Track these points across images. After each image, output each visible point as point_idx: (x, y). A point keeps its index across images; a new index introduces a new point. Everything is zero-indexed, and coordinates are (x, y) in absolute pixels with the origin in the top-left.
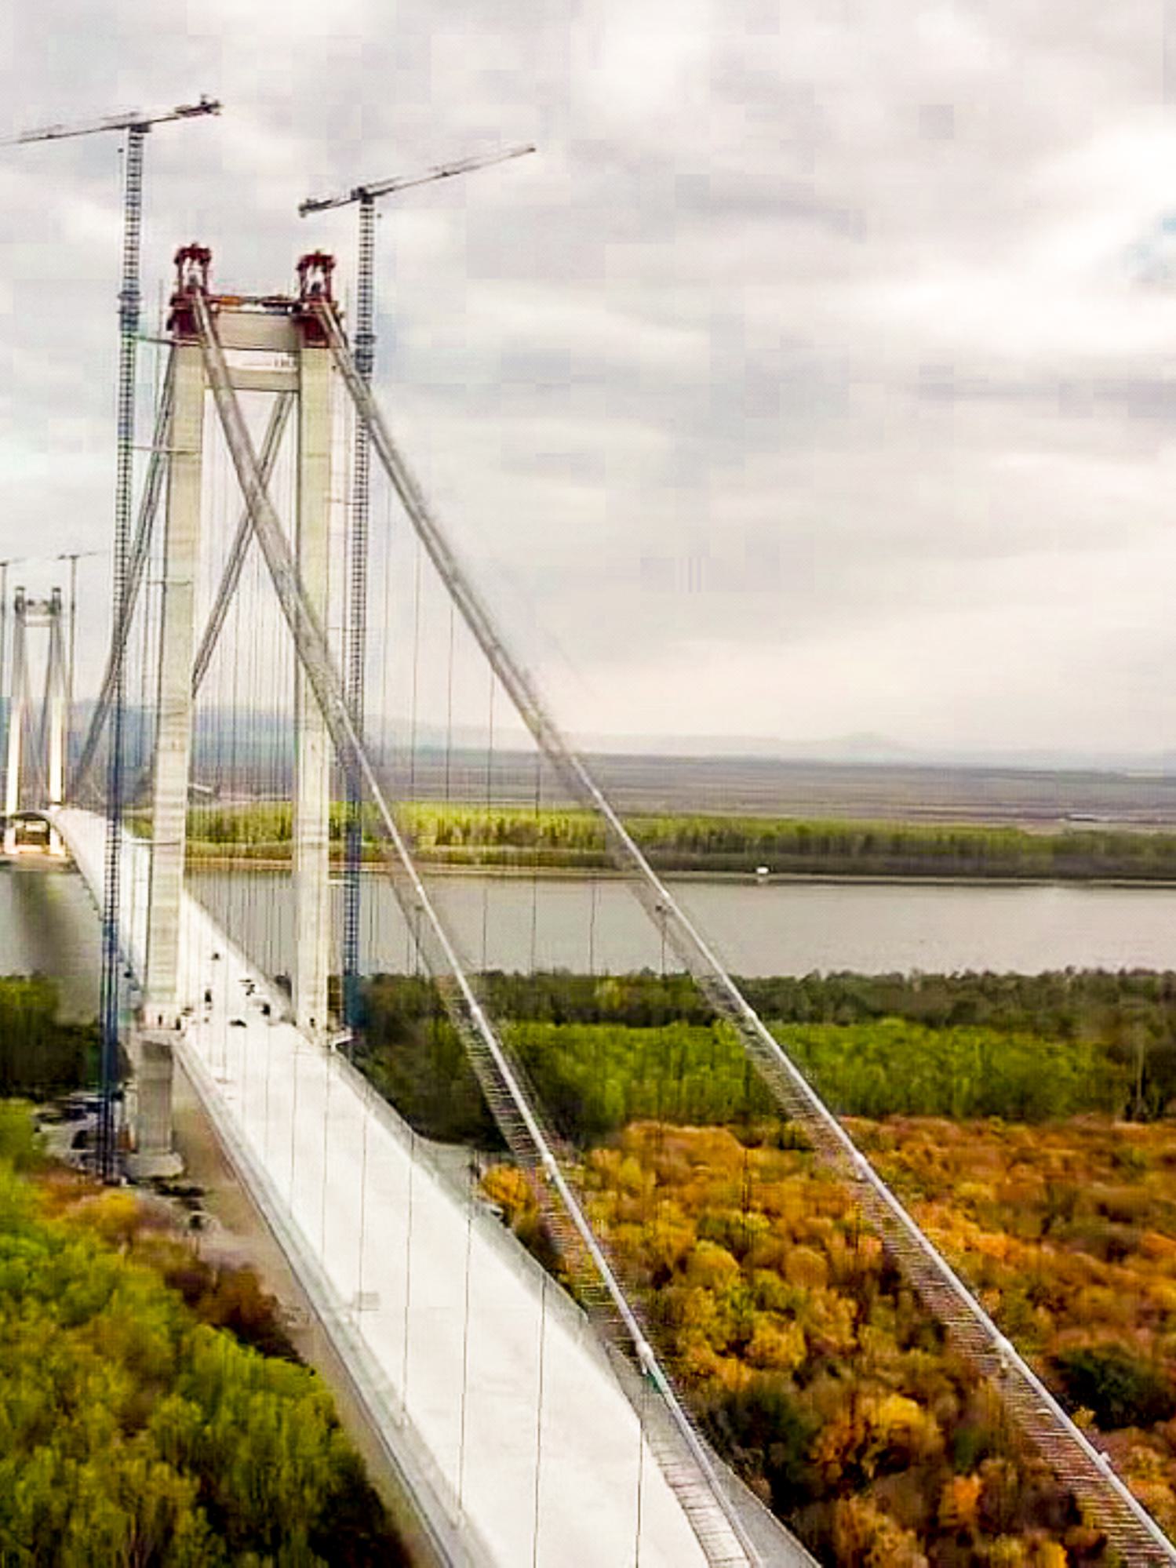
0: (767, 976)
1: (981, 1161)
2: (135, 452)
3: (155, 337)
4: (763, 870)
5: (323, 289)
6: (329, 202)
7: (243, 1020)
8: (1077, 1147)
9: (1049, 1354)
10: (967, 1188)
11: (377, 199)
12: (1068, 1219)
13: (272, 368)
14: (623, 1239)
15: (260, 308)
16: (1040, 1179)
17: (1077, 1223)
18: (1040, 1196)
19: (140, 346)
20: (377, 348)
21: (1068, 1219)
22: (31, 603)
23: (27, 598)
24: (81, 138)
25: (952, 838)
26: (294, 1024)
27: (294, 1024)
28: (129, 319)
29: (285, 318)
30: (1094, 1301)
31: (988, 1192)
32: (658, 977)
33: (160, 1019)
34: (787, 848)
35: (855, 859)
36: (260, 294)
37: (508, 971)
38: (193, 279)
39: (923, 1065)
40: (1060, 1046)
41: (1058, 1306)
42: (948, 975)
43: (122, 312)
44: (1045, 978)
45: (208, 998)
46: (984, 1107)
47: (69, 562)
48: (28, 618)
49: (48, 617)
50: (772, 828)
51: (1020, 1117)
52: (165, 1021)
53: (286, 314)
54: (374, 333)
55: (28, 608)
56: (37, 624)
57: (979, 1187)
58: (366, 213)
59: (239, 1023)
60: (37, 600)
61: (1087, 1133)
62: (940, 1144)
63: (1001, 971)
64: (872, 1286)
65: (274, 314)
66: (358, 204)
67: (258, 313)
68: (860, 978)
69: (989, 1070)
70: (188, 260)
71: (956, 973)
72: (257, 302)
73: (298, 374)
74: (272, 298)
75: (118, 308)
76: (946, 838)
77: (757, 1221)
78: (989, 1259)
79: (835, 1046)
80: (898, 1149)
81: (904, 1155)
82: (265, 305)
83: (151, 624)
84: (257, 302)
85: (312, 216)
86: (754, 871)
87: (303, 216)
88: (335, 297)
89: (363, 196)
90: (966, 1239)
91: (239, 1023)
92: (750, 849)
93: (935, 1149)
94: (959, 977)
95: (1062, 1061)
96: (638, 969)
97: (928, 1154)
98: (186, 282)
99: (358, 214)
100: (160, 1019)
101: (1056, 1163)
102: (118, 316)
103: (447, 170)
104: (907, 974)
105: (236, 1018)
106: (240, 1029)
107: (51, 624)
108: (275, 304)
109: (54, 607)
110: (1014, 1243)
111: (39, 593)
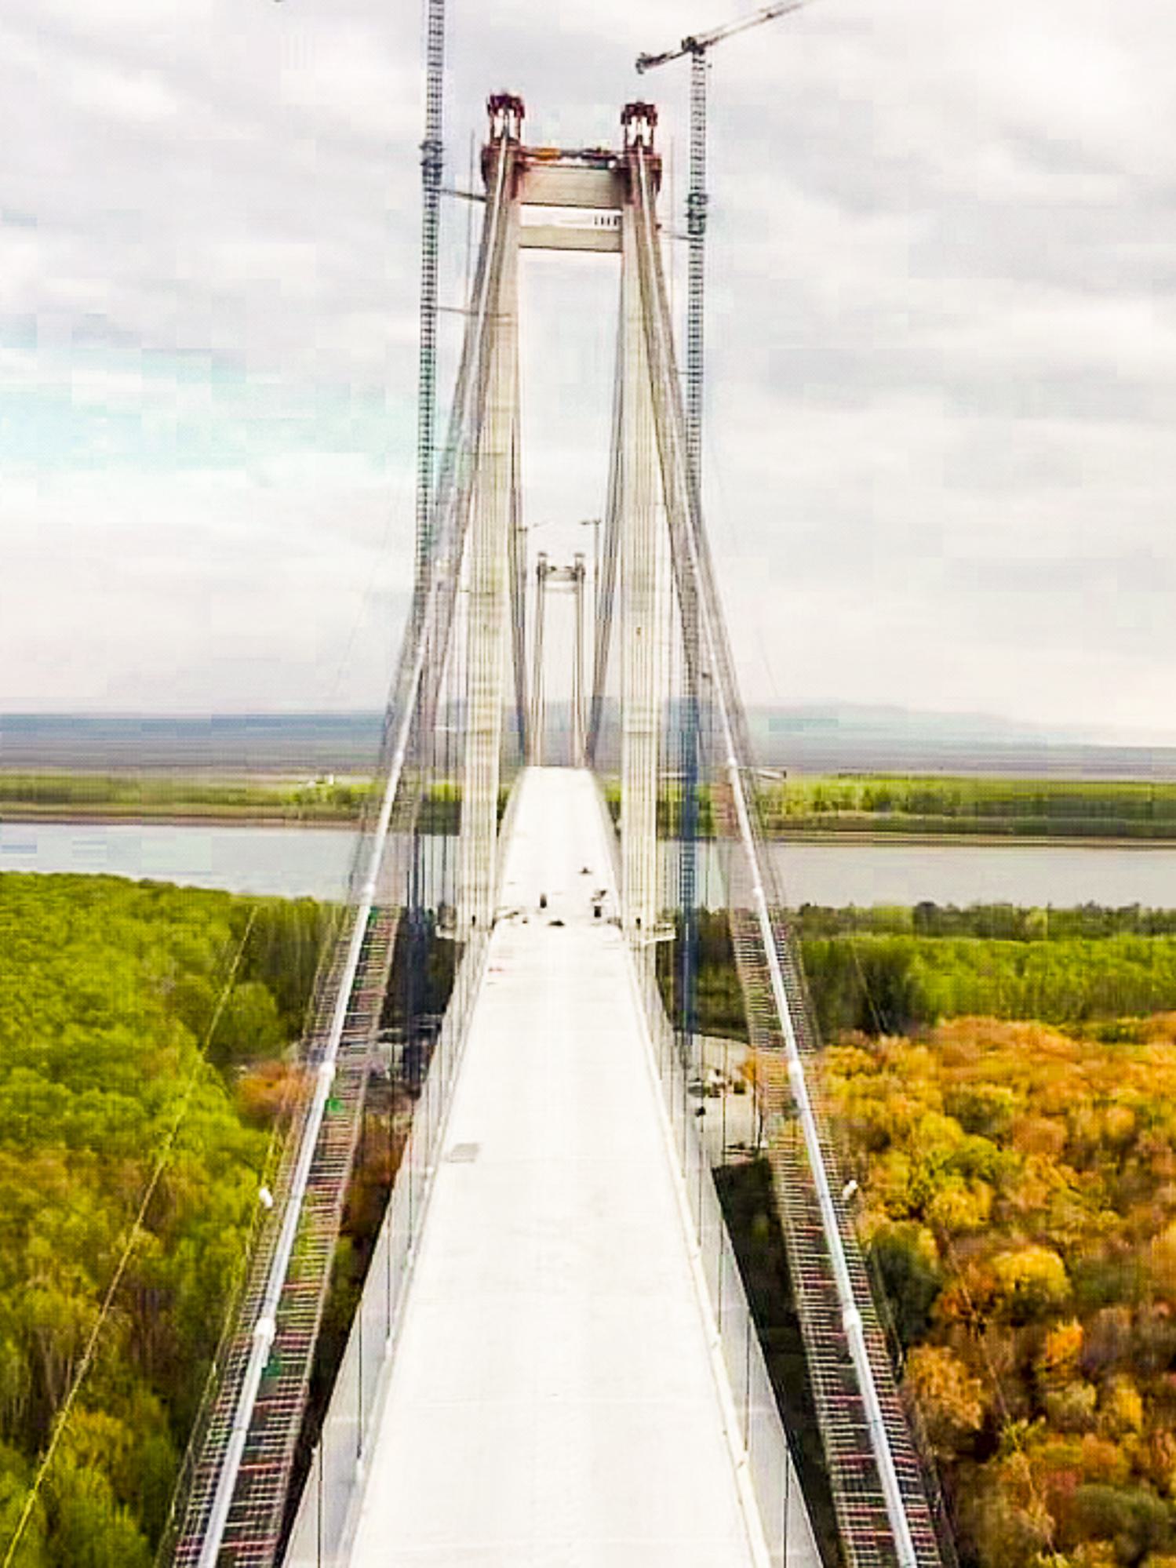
2: (439, 313)
3: (467, 191)
5: (646, 142)
6: (663, 56)
11: (708, 49)
13: (592, 226)
14: (457, 939)
15: (579, 161)
19: (444, 200)
20: (709, 208)
22: (553, 569)
23: (550, 563)
24: (711, 146)
26: (620, 926)
27: (620, 926)
28: (432, 168)
29: (605, 172)
33: (474, 919)
36: (577, 148)
37: (941, 903)
38: (639, 138)
43: (424, 164)
45: (543, 904)
49: (571, 584)
53: (606, 168)
54: (707, 192)
55: (548, 577)
56: (557, 590)
58: (699, 66)
59: (559, 924)
60: (560, 565)
65: (591, 167)
66: (689, 55)
67: (577, 167)
70: (634, 119)
72: (574, 156)
74: (589, 151)
75: (421, 160)
82: (584, 158)
84: (574, 156)
85: (651, 71)
87: (641, 72)
88: (656, 150)
89: (693, 46)
91: (559, 924)
98: (631, 142)
99: (691, 65)
100: (474, 919)
102: (421, 168)
103: (773, 11)
105: (555, 919)
106: (556, 929)
107: (575, 590)
108: (597, 157)
109: (576, 574)
111: (560, 559)
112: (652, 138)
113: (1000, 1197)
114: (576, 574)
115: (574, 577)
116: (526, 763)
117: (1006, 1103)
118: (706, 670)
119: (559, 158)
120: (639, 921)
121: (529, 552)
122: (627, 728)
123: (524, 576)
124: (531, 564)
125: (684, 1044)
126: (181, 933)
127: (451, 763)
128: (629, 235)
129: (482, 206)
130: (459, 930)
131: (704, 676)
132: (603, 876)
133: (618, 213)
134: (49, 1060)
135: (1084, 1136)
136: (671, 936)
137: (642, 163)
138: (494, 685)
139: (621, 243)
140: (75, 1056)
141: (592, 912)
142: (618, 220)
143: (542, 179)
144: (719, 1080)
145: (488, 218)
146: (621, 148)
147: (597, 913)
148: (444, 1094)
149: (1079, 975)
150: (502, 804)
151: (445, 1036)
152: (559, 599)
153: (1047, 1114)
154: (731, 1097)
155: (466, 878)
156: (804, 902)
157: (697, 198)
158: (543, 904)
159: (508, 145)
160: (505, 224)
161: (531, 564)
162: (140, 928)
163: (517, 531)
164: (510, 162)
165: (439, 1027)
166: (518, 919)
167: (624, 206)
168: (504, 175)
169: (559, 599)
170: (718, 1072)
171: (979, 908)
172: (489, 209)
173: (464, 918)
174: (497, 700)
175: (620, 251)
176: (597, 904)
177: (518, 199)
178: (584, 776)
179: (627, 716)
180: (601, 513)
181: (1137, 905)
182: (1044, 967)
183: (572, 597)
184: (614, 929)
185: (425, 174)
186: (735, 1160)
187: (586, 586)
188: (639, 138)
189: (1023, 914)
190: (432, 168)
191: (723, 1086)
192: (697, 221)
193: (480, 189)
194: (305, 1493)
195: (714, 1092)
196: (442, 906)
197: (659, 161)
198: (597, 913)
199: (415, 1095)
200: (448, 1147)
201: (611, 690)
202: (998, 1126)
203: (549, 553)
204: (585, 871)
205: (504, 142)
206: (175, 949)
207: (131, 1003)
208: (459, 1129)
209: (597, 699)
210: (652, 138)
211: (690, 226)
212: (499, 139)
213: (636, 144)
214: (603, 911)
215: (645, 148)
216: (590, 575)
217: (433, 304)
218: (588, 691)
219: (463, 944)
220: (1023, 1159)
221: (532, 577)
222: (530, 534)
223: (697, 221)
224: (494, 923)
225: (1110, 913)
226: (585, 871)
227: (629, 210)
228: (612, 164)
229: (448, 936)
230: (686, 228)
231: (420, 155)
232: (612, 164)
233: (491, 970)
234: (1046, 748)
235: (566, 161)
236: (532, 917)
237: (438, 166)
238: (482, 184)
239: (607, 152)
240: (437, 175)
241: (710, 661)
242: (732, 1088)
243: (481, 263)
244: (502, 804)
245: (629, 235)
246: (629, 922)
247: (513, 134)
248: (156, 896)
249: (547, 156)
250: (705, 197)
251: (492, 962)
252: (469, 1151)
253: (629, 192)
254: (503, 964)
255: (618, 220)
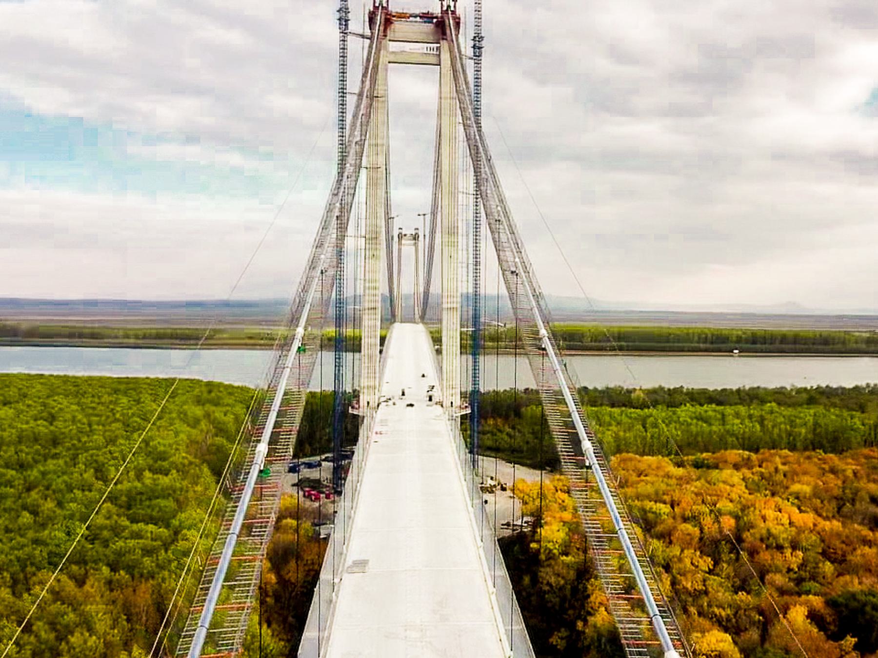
0: (719, 389)
1: (805, 473)
2: (347, 95)
4: (736, 351)
7: (413, 403)
8: (861, 465)
9: (829, 597)
10: (796, 487)
12: (853, 505)
14: (360, 414)
15: (418, 19)
16: (840, 483)
17: (858, 505)
18: (837, 492)
19: (349, 38)
21: (853, 505)
22: (405, 235)
23: (403, 233)
25: (821, 336)
26: (442, 406)
27: (442, 406)
28: (344, 22)
30: (863, 555)
31: (807, 489)
32: (666, 389)
33: (368, 403)
34: (747, 341)
35: (777, 345)
36: (417, 12)
37: (591, 387)
38: (449, 7)
39: (781, 423)
40: (858, 414)
41: (840, 561)
42: (809, 388)
43: (340, 19)
44: (856, 388)
45: (403, 394)
46: (814, 444)
47: (422, 217)
48: (403, 242)
49: (414, 241)
50: (740, 333)
51: (834, 451)
52: (371, 404)
54: (483, 35)
55: (404, 237)
57: (803, 487)
59: (412, 405)
60: (408, 233)
61: (867, 457)
62: (784, 464)
63: (835, 386)
64: (725, 547)
65: (425, 22)
68: (765, 389)
69: (816, 424)
71: (812, 387)
72: (416, 17)
73: (439, 55)
74: (423, 13)
76: (818, 336)
77: (665, 509)
78: (800, 531)
79: (737, 415)
80: (760, 466)
81: (763, 470)
82: (421, 17)
83: (465, 247)
86: (732, 352)
90: (790, 518)
91: (412, 405)
92: (732, 342)
93: (780, 467)
94: (814, 388)
95: (856, 420)
96: (657, 386)
97: (777, 470)
98: (445, 8)
100: (368, 403)
101: (849, 473)
102: (338, 22)
104: (789, 388)
105: (409, 403)
106: (410, 408)
108: (427, 17)
109: (415, 237)
110: (819, 520)
112: (455, 7)
113: (673, 583)
114: (415, 237)
115: (415, 239)
116: (395, 321)
117: (662, 512)
118: (513, 269)
119: (409, 18)
120: (452, 403)
121: (394, 228)
122: (445, 306)
123: (392, 239)
124: (396, 234)
125: (474, 462)
126: (218, 413)
127: (357, 321)
128: (445, 57)
129: (368, 41)
130: (361, 409)
131: (512, 272)
132: (432, 378)
133: (438, 45)
134: (126, 496)
135: (710, 533)
136: (469, 411)
137: (451, 18)
138: (377, 285)
139: (440, 62)
140: (141, 493)
141: (428, 399)
142: (438, 49)
143: (399, 28)
144: (493, 483)
145: (370, 47)
146: (440, 12)
147: (430, 399)
148: (354, 491)
149: (676, 429)
150: (383, 340)
151: (355, 458)
152: (408, 247)
153: (685, 520)
154: (498, 492)
155: (364, 382)
156: (527, 387)
157: (478, 38)
158: (403, 394)
159: (382, 9)
160: (380, 50)
161: (396, 234)
162: (198, 411)
163: (389, 219)
164: (383, 17)
165: (353, 453)
166: (391, 403)
167: (441, 42)
168: (380, 22)
169: (408, 247)
170: (492, 478)
171: (607, 388)
172: (372, 42)
173: (363, 399)
174: (379, 292)
175: (440, 65)
176: (430, 393)
177: (388, 38)
178: (421, 327)
179: (445, 300)
180: (428, 211)
181: (682, 387)
182: (655, 425)
183: (413, 248)
184: (439, 407)
185: (340, 24)
186: (508, 533)
187: (420, 243)
188: (449, 7)
189: (629, 392)
190: (344, 22)
191: (495, 486)
192: (477, 49)
193: (368, 32)
194: (327, 551)
195: (491, 490)
196: (354, 391)
197: (459, 18)
198: (430, 399)
199: (339, 493)
200: (349, 562)
201: (434, 289)
202: (659, 528)
203: (386, 407)
204: (423, 376)
205: (380, 8)
206: (214, 422)
207: (181, 456)
208: (354, 551)
209: (426, 294)
210: (455, 7)
211: (474, 53)
212: (378, 7)
213: (447, 10)
214: (433, 398)
215: (452, 11)
216: (421, 238)
217: (345, 91)
218: (421, 290)
219: (364, 417)
220: (682, 551)
221: (396, 239)
222: (395, 220)
223: (477, 49)
224: (378, 406)
225: (669, 390)
226: (423, 376)
227: (444, 44)
228: (435, 20)
229: (355, 412)
230: (472, 54)
231: (338, 15)
232: (435, 20)
233: (376, 433)
234: (609, 312)
235: (411, 19)
236: (396, 400)
237: (346, 21)
238: (369, 31)
239: (432, 14)
240: (346, 25)
241: (516, 263)
242: (499, 487)
243: (368, 60)
244: (383, 340)
245: (445, 57)
246: (447, 403)
247: (385, 5)
248: (210, 392)
249: (402, 16)
250: (482, 37)
251: (377, 428)
252: (361, 564)
253: (444, 33)
254: (383, 429)
255: (438, 49)
